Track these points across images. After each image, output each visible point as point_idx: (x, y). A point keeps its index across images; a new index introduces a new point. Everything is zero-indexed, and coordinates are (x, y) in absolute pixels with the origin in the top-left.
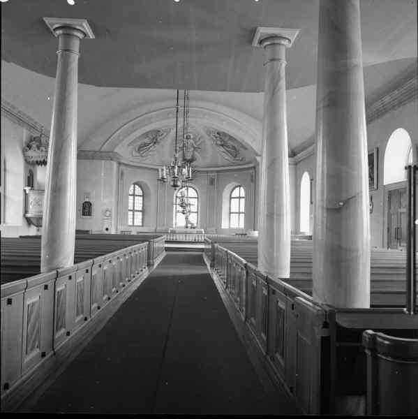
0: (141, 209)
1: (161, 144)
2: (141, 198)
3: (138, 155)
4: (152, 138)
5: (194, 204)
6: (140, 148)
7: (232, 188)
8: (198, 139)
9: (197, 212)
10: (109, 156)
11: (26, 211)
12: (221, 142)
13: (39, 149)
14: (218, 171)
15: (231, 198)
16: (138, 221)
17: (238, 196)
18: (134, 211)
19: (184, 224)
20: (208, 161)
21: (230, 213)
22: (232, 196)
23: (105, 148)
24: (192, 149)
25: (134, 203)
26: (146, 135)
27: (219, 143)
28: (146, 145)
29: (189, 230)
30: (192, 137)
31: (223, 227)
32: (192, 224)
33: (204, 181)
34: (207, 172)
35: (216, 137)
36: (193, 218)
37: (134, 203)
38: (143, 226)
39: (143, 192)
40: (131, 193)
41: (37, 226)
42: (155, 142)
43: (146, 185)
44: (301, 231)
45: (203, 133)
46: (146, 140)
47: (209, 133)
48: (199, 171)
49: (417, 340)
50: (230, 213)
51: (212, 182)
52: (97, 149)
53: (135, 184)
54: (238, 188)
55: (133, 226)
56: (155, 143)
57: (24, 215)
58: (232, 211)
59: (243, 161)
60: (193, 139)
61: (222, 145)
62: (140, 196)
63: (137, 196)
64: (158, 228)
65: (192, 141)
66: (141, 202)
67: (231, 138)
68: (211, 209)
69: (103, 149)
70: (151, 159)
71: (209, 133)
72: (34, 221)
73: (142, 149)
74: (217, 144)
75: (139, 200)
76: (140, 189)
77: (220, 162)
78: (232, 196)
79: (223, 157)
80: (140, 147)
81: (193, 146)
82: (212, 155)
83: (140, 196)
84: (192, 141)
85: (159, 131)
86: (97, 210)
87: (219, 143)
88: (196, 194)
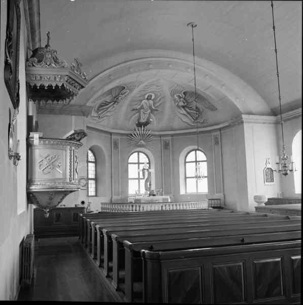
1: (120, 104)
4: (114, 96)
7: (185, 155)
9: (186, 178)
14: (172, 135)
15: (185, 162)
20: (164, 123)
22: (187, 161)
24: (149, 111)
27: (181, 104)
28: (106, 104)
30: (153, 97)
34: (160, 136)
35: (180, 98)
38: (96, 195)
39: (95, 159)
44: (135, 193)
45: (168, 93)
46: (108, 99)
51: (166, 146)
54: (194, 152)
56: (115, 102)
57: (28, 189)
59: (204, 124)
60: (153, 100)
61: (183, 107)
65: (151, 102)
68: (167, 174)
77: (176, 124)
79: (181, 119)
80: (101, 106)
81: (150, 107)
88: (147, 159)
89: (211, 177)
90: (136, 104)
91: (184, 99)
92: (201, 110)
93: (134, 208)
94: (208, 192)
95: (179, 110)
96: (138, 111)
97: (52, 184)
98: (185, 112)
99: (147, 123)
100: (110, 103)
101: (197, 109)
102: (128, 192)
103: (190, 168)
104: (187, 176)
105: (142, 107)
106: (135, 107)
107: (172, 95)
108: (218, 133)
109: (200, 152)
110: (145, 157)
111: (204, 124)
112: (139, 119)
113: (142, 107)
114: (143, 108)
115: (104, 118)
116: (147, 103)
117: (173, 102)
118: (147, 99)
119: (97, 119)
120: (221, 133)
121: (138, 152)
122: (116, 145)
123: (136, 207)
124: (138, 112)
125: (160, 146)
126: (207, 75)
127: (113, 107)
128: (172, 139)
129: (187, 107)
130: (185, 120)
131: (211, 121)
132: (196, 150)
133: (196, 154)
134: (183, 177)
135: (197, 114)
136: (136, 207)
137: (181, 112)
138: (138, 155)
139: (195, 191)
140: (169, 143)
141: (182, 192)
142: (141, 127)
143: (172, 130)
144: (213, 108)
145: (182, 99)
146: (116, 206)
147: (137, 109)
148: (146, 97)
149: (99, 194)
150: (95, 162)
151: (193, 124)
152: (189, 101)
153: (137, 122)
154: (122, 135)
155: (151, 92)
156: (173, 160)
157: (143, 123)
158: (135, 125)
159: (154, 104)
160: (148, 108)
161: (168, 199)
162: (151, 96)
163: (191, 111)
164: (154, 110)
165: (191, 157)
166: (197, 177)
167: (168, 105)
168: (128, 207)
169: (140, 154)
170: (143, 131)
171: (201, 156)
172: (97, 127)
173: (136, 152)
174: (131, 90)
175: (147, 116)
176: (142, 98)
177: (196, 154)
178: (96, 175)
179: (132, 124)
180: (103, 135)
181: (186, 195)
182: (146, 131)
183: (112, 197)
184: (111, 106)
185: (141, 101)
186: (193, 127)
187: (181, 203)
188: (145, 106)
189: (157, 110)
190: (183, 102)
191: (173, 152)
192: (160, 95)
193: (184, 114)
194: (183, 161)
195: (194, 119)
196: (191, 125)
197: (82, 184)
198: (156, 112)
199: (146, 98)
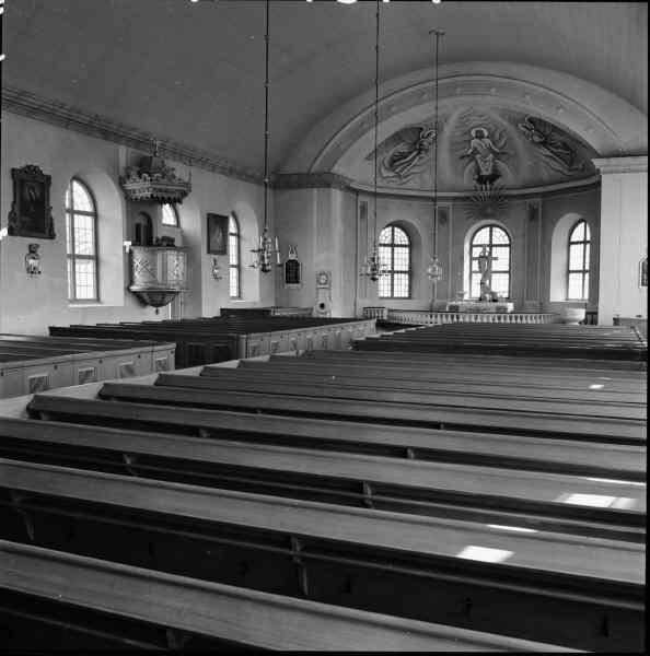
0: (406, 268)
2: (407, 250)
3: (392, 174)
5: (502, 259)
6: (393, 162)
7: (572, 223)
8: (497, 136)
10: (325, 180)
11: (131, 281)
12: (540, 137)
13: (140, 177)
14: (544, 195)
16: (402, 288)
17: (582, 239)
18: (393, 272)
19: (477, 293)
20: (525, 175)
21: (569, 272)
22: (572, 240)
23: (316, 167)
25: (393, 259)
26: (397, 137)
28: (403, 156)
29: (482, 305)
30: (486, 133)
31: (551, 300)
32: (493, 294)
33: (519, 213)
36: (501, 285)
37: (393, 259)
38: (410, 297)
40: (588, 246)
41: (154, 305)
42: (418, 148)
43: (417, 232)
46: (402, 148)
47: (515, 121)
48: (507, 197)
49: (641, 607)
50: (569, 272)
52: (305, 171)
53: (393, 225)
55: (392, 297)
56: (420, 150)
57: (128, 289)
58: (571, 268)
61: (544, 144)
62: (405, 246)
63: (398, 246)
64: (437, 301)
66: (407, 256)
67: (555, 128)
69: (313, 171)
70: (419, 179)
71: (515, 121)
72: (146, 297)
73: (398, 163)
74: (533, 141)
75: (402, 255)
76: (403, 234)
77: (545, 174)
78: (572, 240)
79: (547, 166)
81: (490, 149)
82: (527, 166)
83: (405, 246)
84: (488, 141)
85: (422, 129)
86: (308, 272)
87: (537, 139)
88: (406, 239)
94: (589, 300)
96: (472, 157)
97: (150, 285)
98: (548, 153)
99: (495, 176)
100: (410, 153)
104: (571, 268)
106: (463, 152)
109: (498, 230)
112: (478, 171)
113: (475, 151)
114: (479, 153)
119: (397, 179)
121: (491, 226)
122: (364, 209)
124: (471, 161)
126: (527, 94)
134: (564, 269)
138: (491, 231)
140: (537, 209)
148: (473, 133)
151: (570, 173)
153: (476, 177)
154: (455, 199)
158: (475, 182)
159: (494, 143)
168: (449, 318)
169: (494, 229)
171: (500, 236)
174: (438, 128)
175: (490, 166)
176: (467, 137)
178: (410, 267)
179: (467, 181)
180: (415, 203)
183: (433, 300)
184: (414, 157)
185: (469, 141)
188: (479, 149)
189: (504, 153)
197: (323, 281)
198: (504, 158)
199: (474, 135)
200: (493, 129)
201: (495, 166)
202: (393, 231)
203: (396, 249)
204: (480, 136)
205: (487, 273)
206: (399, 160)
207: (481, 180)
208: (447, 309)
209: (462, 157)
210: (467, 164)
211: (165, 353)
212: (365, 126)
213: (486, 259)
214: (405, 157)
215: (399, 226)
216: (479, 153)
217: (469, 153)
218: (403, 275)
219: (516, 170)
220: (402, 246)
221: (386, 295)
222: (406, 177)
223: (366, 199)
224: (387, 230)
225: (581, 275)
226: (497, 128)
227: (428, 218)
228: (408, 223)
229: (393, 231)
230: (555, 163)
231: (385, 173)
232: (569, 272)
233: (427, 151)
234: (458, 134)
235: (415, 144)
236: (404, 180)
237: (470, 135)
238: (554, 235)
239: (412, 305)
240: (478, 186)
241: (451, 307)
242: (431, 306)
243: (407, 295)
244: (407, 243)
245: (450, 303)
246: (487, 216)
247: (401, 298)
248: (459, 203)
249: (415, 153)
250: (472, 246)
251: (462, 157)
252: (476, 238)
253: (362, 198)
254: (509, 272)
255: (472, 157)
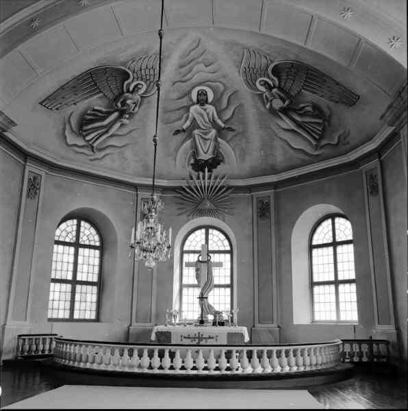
3: (81, 142)
4: (111, 96)
14: (275, 185)
16: (87, 301)
20: (254, 158)
22: (314, 243)
24: (214, 132)
25: (76, 263)
27: (278, 104)
28: (98, 116)
31: (296, 322)
32: (217, 313)
33: (246, 211)
34: (250, 189)
36: (220, 300)
37: (76, 263)
38: (97, 320)
45: (237, 80)
46: (97, 102)
51: (263, 210)
53: (80, 216)
55: (71, 319)
61: (285, 111)
62: (94, 247)
63: (85, 246)
76: (93, 231)
77: (279, 157)
78: (314, 243)
84: (211, 109)
87: (278, 104)
88: (97, 238)
89: (362, 281)
90: (180, 119)
91: (280, 88)
92: (326, 110)
93: (178, 362)
95: (280, 122)
96: (188, 133)
98: (292, 126)
101: (317, 111)
102: (330, 322)
103: (322, 258)
105: (194, 125)
106: (177, 125)
107: (251, 83)
108: (375, 163)
109: (216, 232)
110: (222, 237)
111: (342, 147)
112: (195, 153)
113: (194, 125)
114: (199, 128)
115: (107, 151)
116: (203, 112)
117: (260, 104)
118: (198, 102)
120: (381, 162)
121: (207, 228)
122: (34, 186)
123: (183, 357)
125: (250, 213)
127: (122, 125)
128: (275, 193)
129: (295, 111)
130: (298, 144)
131: (354, 136)
132: (333, 216)
133: (333, 224)
134: (307, 283)
135: (318, 124)
136: (183, 357)
137: (285, 126)
138: (207, 234)
139: (334, 318)
140: (268, 204)
141: (300, 317)
142: (204, 172)
143: (274, 171)
144: (350, 99)
145: (275, 90)
146: (73, 347)
147: (184, 131)
148: (195, 98)
149: (102, 317)
150: (102, 248)
151: (316, 153)
152: (293, 93)
153: (192, 161)
155: (200, 84)
156: (279, 245)
157: (206, 161)
158: (190, 169)
159: (219, 113)
160: (210, 125)
161: (242, 336)
162: (206, 94)
163: (307, 119)
164: (224, 128)
165: (323, 234)
166: (337, 283)
167: (252, 110)
170: (209, 178)
171: (217, 240)
172: (83, 169)
173: (199, 228)
175: (210, 146)
176: (185, 102)
177: (333, 224)
181: (315, 326)
182: (216, 178)
185: (187, 109)
186: (318, 158)
187: (266, 349)
188: (199, 121)
189: (230, 129)
190: (281, 98)
191: (278, 223)
192: (226, 88)
193: (293, 131)
194: (305, 244)
195: (315, 139)
196: (311, 156)
198: (231, 134)
199: (195, 99)
200: (221, 87)
201: (216, 148)
202: (79, 226)
203: (81, 250)
204: (202, 100)
205: (206, 285)
206: (91, 121)
207: (199, 166)
208: (153, 337)
209: (177, 132)
210: (183, 142)
211: (358, 350)
212: (36, 24)
213: (204, 265)
214: (104, 119)
215: (87, 220)
216: (199, 128)
217: (185, 127)
218: (89, 287)
219: (243, 154)
220: (90, 247)
221: (61, 316)
222: (100, 150)
223: (42, 171)
224: (69, 222)
225: (333, 287)
226: (226, 88)
227: (127, 212)
228: (104, 218)
229: (79, 226)
230: (299, 140)
231: (71, 139)
232: (313, 284)
233: (131, 115)
234: (175, 95)
235: (116, 99)
236: (99, 155)
237: (191, 100)
238: (293, 235)
239: (101, 332)
240: (194, 174)
241: (159, 334)
242: (128, 333)
243: (93, 317)
244: (98, 244)
245: (156, 329)
246: (202, 213)
247: (85, 320)
248: (169, 195)
249: (116, 114)
250: (182, 253)
251: (177, 132)
252: (187, 242)
253: (31, 168)
254: (231, 286)
255: (188, 133)
